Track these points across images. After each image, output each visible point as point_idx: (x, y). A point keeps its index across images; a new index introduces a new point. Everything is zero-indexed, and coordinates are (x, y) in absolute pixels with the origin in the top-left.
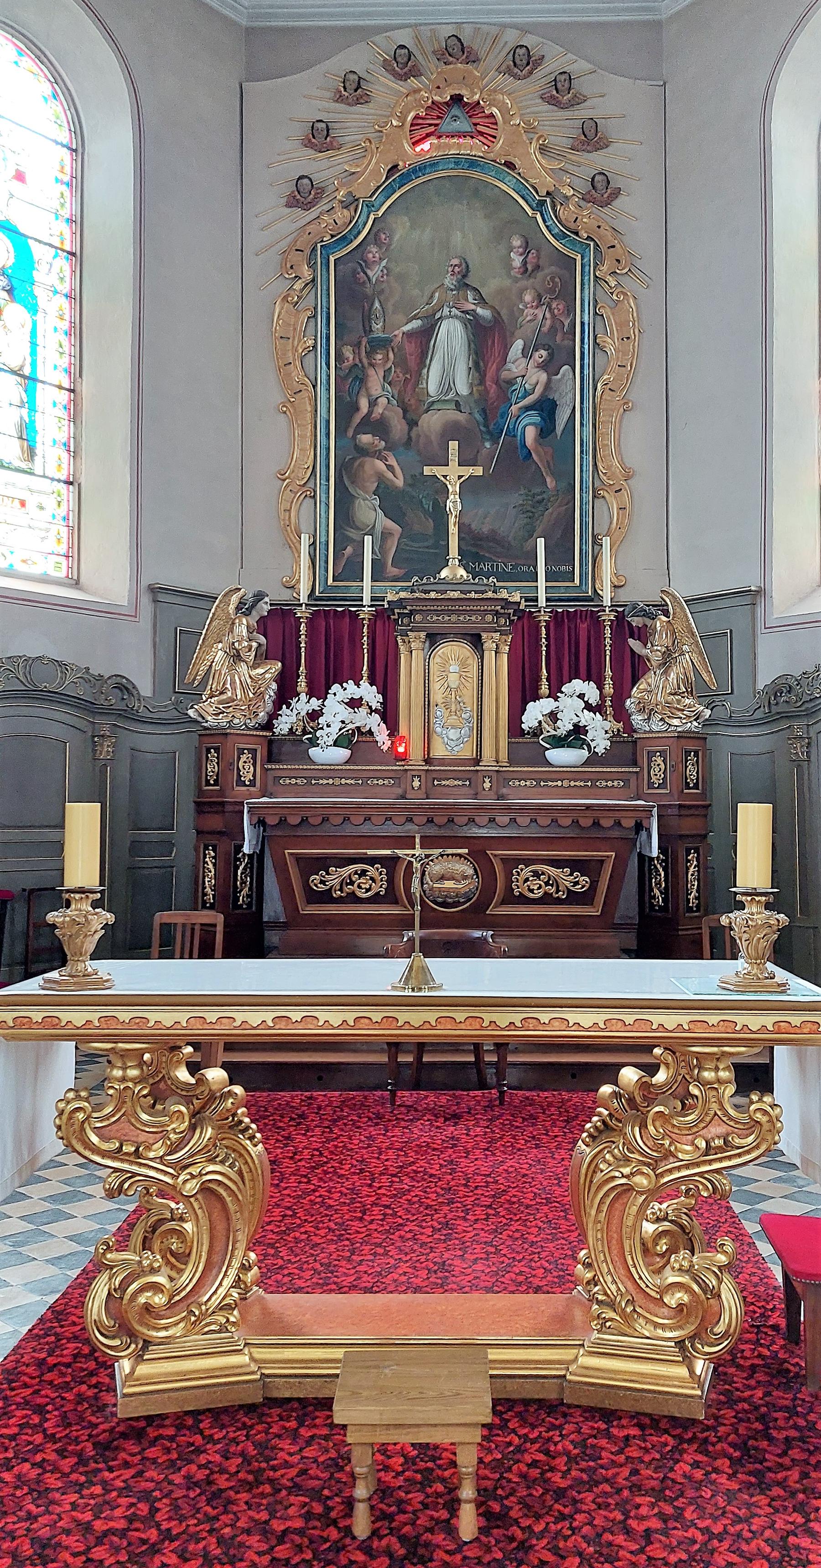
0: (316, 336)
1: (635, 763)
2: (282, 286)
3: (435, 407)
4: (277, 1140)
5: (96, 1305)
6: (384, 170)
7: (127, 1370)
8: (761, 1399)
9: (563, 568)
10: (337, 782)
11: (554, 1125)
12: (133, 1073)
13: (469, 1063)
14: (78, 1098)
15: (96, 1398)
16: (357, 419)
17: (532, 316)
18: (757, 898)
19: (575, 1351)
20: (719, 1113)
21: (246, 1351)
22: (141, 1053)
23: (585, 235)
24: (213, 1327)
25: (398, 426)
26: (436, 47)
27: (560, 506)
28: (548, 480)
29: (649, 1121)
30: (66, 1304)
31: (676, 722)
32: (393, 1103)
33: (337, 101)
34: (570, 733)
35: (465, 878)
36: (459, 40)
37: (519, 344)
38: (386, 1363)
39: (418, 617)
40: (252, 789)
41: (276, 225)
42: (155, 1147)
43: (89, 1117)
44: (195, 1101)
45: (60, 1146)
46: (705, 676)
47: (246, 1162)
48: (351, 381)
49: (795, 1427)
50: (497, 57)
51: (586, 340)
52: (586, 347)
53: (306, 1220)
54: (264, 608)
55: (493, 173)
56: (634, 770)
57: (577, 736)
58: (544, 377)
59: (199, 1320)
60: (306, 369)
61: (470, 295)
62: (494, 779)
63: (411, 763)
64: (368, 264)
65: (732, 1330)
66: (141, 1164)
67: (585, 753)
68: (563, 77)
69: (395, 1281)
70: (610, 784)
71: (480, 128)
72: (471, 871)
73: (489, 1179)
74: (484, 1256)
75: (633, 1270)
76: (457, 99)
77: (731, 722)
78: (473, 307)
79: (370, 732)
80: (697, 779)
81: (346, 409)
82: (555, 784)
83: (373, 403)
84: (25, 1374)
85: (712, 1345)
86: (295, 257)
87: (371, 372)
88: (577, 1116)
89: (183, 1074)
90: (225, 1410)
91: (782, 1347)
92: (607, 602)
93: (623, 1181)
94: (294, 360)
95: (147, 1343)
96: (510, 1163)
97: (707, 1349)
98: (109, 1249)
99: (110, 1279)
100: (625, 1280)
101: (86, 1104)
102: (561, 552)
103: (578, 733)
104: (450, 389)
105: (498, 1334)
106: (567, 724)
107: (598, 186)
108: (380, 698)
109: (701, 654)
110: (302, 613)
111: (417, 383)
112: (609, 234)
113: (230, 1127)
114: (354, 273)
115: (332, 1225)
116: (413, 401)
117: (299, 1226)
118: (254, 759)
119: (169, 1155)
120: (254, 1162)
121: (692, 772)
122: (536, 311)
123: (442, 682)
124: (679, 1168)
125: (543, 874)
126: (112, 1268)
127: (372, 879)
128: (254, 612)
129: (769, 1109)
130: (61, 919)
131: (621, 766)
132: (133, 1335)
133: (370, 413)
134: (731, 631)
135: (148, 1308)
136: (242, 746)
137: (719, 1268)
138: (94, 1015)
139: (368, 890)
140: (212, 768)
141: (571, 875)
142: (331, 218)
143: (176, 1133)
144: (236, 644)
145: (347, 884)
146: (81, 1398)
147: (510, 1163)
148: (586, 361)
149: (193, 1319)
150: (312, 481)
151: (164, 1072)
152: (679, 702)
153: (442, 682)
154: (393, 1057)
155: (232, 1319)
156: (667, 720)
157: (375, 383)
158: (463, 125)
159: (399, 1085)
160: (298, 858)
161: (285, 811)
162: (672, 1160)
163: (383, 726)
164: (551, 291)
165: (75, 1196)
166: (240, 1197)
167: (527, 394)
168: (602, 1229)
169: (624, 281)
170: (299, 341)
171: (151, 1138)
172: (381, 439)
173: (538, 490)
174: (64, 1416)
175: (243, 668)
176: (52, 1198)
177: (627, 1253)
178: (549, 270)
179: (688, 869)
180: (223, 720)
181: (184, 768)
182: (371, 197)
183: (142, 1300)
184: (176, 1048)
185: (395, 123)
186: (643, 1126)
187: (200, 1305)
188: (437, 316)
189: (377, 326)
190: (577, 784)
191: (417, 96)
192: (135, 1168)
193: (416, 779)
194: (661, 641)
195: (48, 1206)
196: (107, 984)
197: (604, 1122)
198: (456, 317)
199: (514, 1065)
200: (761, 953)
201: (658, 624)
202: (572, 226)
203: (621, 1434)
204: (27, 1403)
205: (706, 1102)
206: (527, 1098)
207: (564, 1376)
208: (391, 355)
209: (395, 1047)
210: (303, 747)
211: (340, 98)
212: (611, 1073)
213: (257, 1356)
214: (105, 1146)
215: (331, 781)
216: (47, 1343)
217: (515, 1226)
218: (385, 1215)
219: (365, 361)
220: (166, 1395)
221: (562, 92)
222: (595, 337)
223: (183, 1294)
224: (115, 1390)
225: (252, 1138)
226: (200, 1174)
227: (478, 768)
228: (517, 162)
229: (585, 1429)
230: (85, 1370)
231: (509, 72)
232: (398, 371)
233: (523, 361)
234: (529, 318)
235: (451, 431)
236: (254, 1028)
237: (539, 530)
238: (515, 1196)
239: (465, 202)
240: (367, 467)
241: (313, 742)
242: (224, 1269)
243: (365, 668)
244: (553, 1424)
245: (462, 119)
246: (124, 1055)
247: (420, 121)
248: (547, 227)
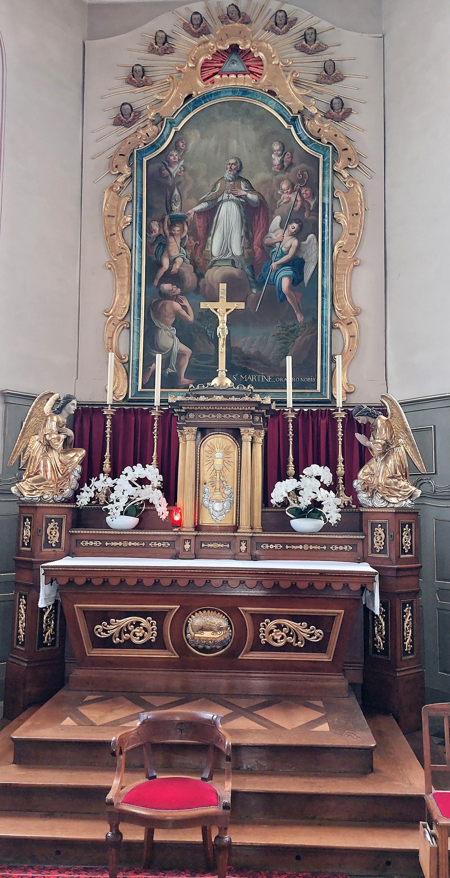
0: (133, 215)
1: (360, 530)
2: (109, 180)
3: (218, 264)
6: (183, 96)
9: (308, 379)
10: (125, 544)
16: (161, 273)
17: (287, 198)
23: (326, 142)
25: (190, 277)
26: (221, 13)
27: (307, 334)
28: (298, 316)
31: (393, 500)
33: (150, 52)
34: (309, 507)
35: (220, 629)
36: (237, 8)
37: (277, 220)
39: (191, 415)
40: (57, 550)
41: (106, 137)
46: (416, 463)
48: (157, 246)
50: (265, 19)
51: (326, 216)
52: (326, 220)
54: (72, 408)
55: (260, 98)
57: (315, 508)
58: (295, 242)
60: (126, 238)
61: (243, 185)
63: (184, 529)
64: (170, 164)
68: (310, 31)
70: (341, 548)
71: (251, 69)
72: (225, 624)
76: (234, 49)
77: (434, 495)
78: (245, 193)
80: (411, 546)
81: (153, 265)
82: (297, 547)
83: (172, 262)
86: (119, 160)
87: (171, 239)
92: (339, 404)
94: (117, 231)
102: (305, 369)
103: (315, 508)
104: (228, 251)
106: (306, 500)
107: (336, 106)
108: (161, 478)
109: (413, 446)
110: (108, 412)
111: (204, 247)
112: (343, 140)
114: (160, 170)
116: (201, 260)
118: (60, 526)
121: (407, 540)
122: (290, 196)
123: (209, 465)
125: (285, 626)
127: (145, 629)
128: (64, 412)
133: (170, 268)
134: (434, 426)
136: (48, 516)
139: (141, 638)
140: (27, 533)
141: (308, 628)
142: (144, 132)
144: (47, 436)
145: (125, 633)
148: (326, 231)
150: (128, 317)
152: (396, 484)
153: (209, 465)
157: (174, 247)
158: (238, 66)
160: (85, 612)
161: (73, 574)
164: (300, 181)
167: (283, 254)
169: (352, 172)
170: (121, 218)
172: (178, 287)
173: (291, 323)
175: (54, 455)
178: (299, 167)
179: (404, 620)
180: (36, 496)
182: (173, 116)
185: (190, 65)
188: (219, 199)
189: (176, 208)
190: (315, 547)
191: (207, 46)
193: (187, 543)
194: (381, 435)
198: (233, 200)
201: (379, 422)
202: (316, 135)
208: (186, 228)
211: (152, 50)
215: (120, 544)
219: (167, 232)
221: (310, 42)
222: (333, 214)
227: (236, 534)
228: (277, 90)
231: (272, 29)
232: (191, 238)
233: (280, 232)
234: (285, 200)
235: (228, 279)
237: (291, 352)
239: (240, 119)
240: (168, 307)
243: (155, 453)
245: (239, 62)
247: (209, 65)
248: (299, 136)
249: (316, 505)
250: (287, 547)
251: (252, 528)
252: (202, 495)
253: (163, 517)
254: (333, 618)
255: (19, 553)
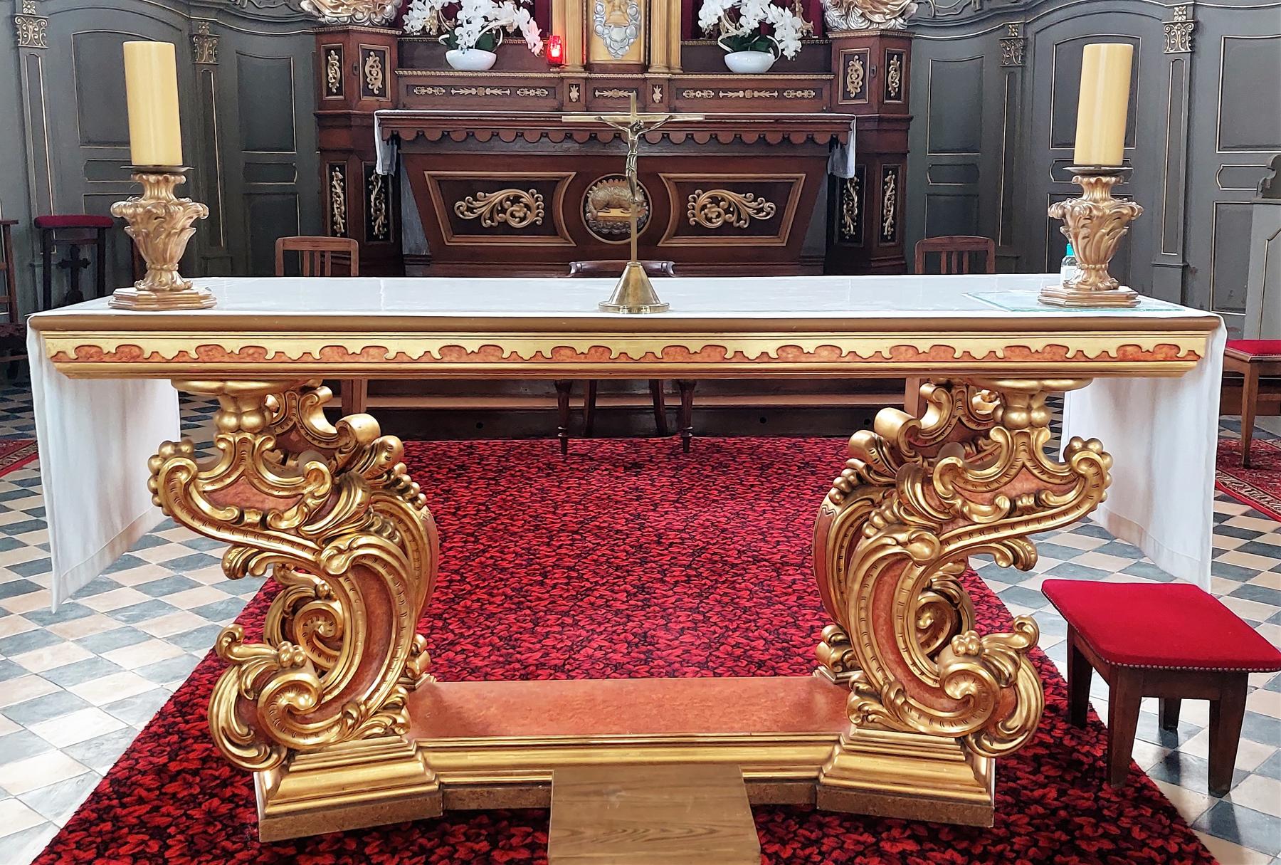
1: (829, 71)
4: (436, 494)
5: (223, 704)
7: (269, 785)
8: (1055, 799)
10: (481, 92)
11: (747, 473)
12: (252, 420)
13: (646, 408)
14: (178, 453)
15: (232, 817)
18: (1104, 179)
19: (829, 749)
20: (1028, 464)
21: (419, 756)
22: (260, 397)
24: (376, 730)
29: (936, 476)
30: (192, 693)
31: (877, 18)
32: (564, 451)
34: (755, 32)
38: (611, 787)
40: (381, 99)
42: (287, 515)
43: (194, 478)
44: (338, 455)
45: (159, 516)
47: (408, 529)
49: (1106, 835)
53: (477, 586)
56: (828, 77)
59: (358, 722)
62: (666, 88)
63: (568, 69)
65: (1030, 724)
66: (270, 537)
67: (770, 58)
69: (590, 657)
70: (799, 94)
73: (684, 535)
74: (689, 625)
75: (905, 655)
79: (518, 33)
80: (900, 87)
82: (736, 94)
84: (141, 785)
85: (1003, 741)
88: (772, 464)
89: (319, 422)
90: (396, 828)
91: (1067, 732)
93: (898, 549)
95: (293, 753)
96: (706, 516)
97: (997, 746)
98: (235, 641)
99: (239, 677)
100: (894, 666)
101: (189, 462)
103: (763, 36)
105: (732, 729)
106: (751, 21)
113: (385, 487)
115: (509, 591)
117: (470, 593)
118: (383, 62)
119: (307, 524)
120: (422, 538)
121: (894, 78)
124: (970, 534)
125: (723, 200)
126: (240, 664)
127: (527, 206)
129: (1097, 457)
130: (130, 211)
131: (814, 73)
132: (273, 744)
135: (291, 711)
137: (1017, 652)
138: (189, 343)
139: (522, 219)
140: (333, 73)
141: (755, 200)
143: (314, 497)
146: (211, 817)
147: (706, 516)
149: (350, 722)
151: (295, 419)
154: (564, 403)
155: (400, 720)
156: (868, 15)
159: (569, 433)
160: (440, 181)
162: (962, 522)
163: (533, 23)
165: (201, 561)
166: (404, 575)
168: (866, 608)
171: (281, 505)
174: (191, 841)
176: (175, 564)
177: (897, 635)
179: (884, 193)
181: (300, 76)
183: (283, 701)
184: (308, 390)
186: (927, 482)
187: (358, 705)
190: (762, 94)
192: (262, 543)
193: (574, 90)
195: (168, 573)
196: (205, 303)
197: (858, 476)
199: (698, 408)
200: (1102, 254)
203: (895, 850)
204: (142, 824)
205: (1011, 451)
206: (713, 444)
207: (817, 778)
209: (565, 387)
210: (439, 51)
212: (866, 419)
213: (433, 762)
214: (220, 515)
215: (473, 91)
216: (169, 744)
217: (723, 589)
218: (569, 578)
220: (320, 814)
223: (336, 693)
224: (255, 805)
225: (413, 500)
226: (350, 549)
227: (647, 75)
229: (849, 845)
230: (217, 778)
236: (415, 362)
238: (715, 554)
241: (452, 44)
242: (387, 662)
244: (807, 838)
246: (237, 397)
249: (766, 29)
250: (721, 94)
251: (669, 67)
252: (592, 17)
253: (536, 50)
254: (789, 185)
255: (322, 104)
